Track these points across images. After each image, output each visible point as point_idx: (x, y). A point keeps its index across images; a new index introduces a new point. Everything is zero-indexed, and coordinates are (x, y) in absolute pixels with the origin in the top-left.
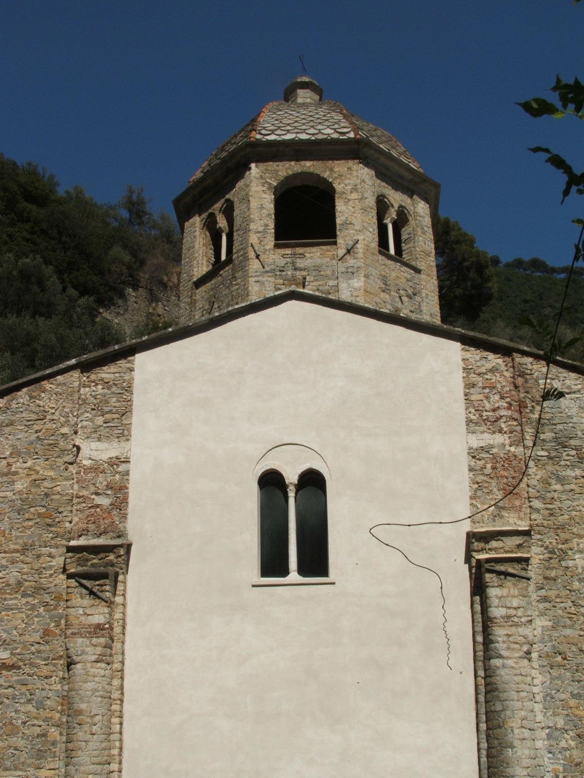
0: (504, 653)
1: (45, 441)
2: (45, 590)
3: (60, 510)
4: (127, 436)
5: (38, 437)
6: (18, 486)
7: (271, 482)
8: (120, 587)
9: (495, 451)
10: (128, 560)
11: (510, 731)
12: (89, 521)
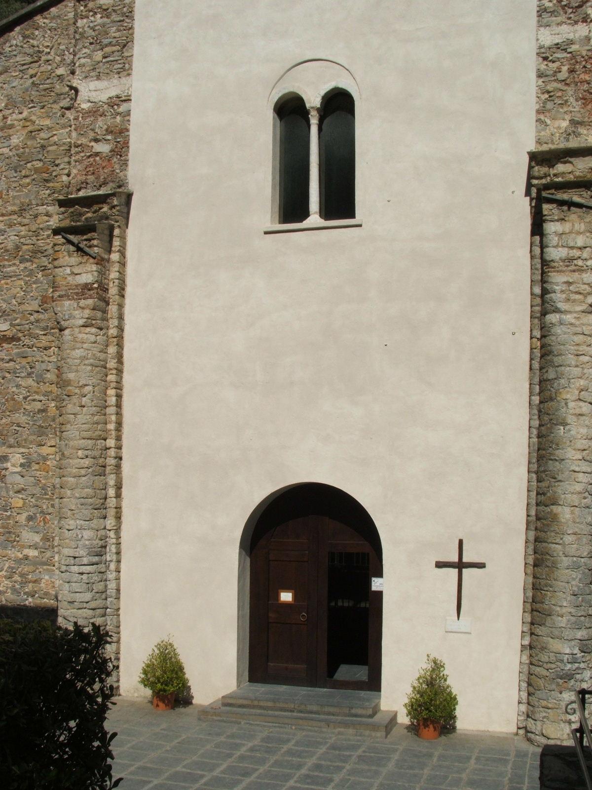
0: (560, 305)
1: (41, 86)
2: (42, 253)
3: (57, 162)
4: (128, 70)
5: (33, 83)
6: (15, 141)
8: (116, 242)
9: (574, 48)
10: (128, 213)
11: (563, 404)
12: (87, 172)
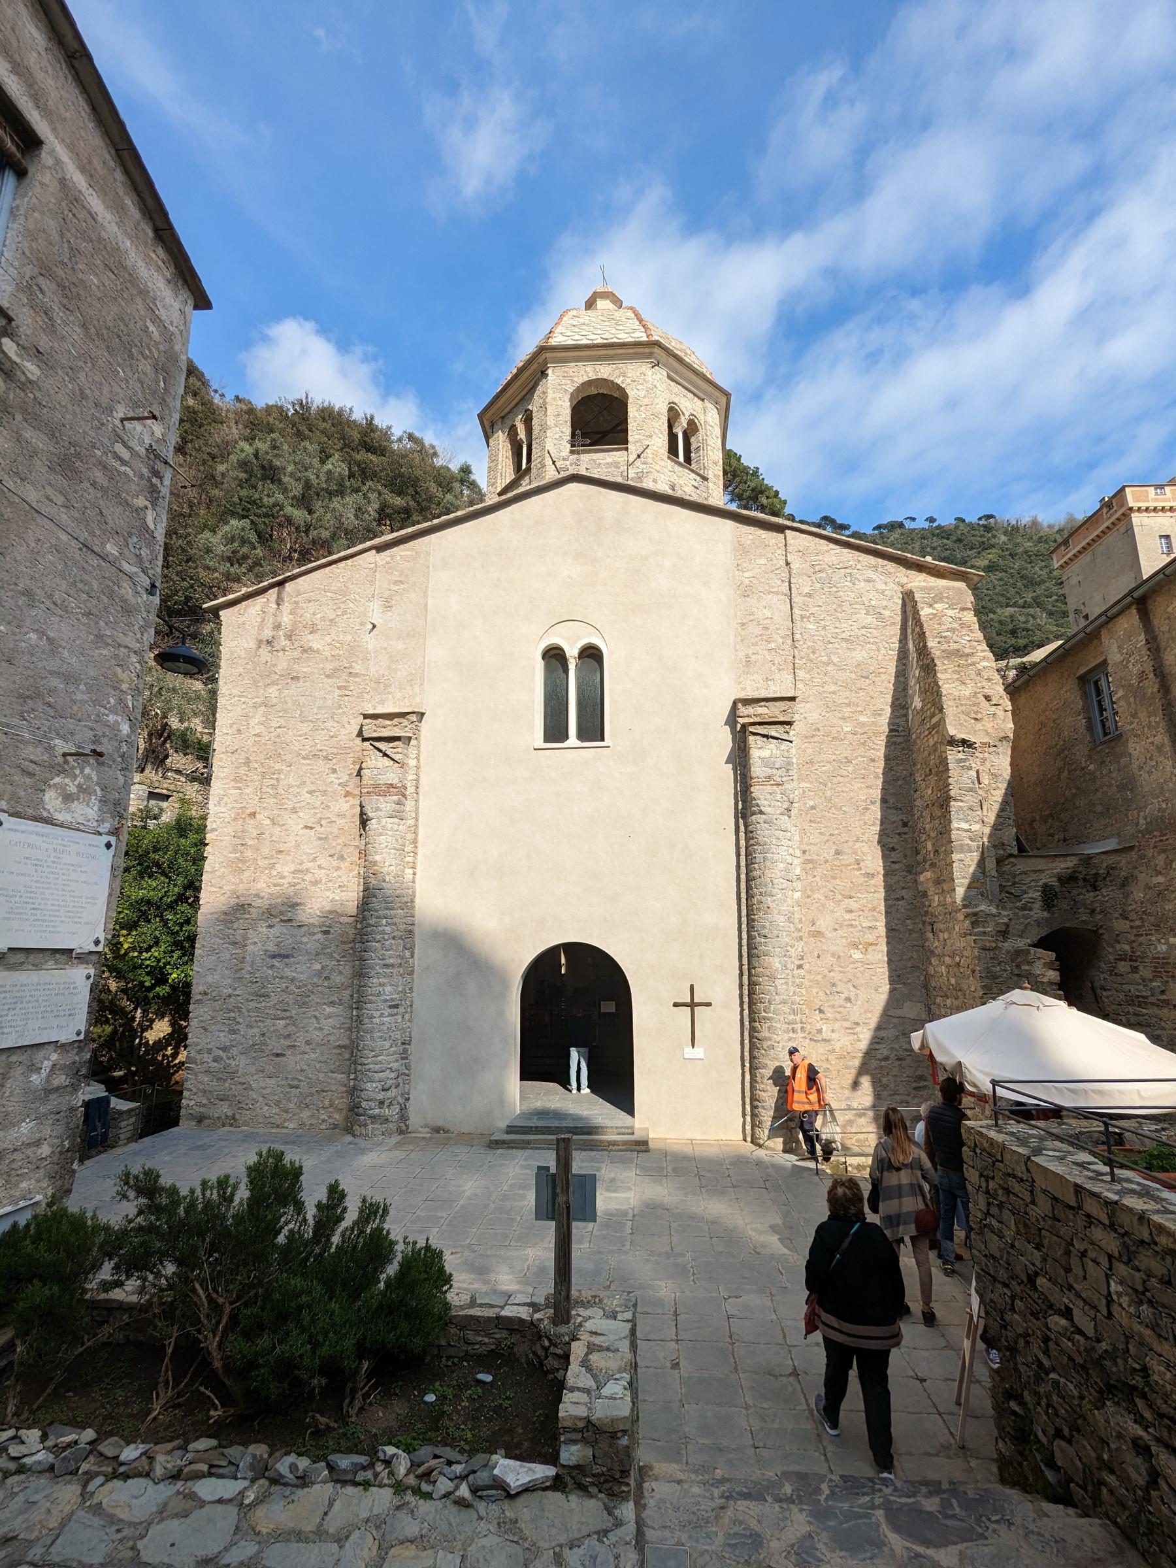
7: (554, 656)
